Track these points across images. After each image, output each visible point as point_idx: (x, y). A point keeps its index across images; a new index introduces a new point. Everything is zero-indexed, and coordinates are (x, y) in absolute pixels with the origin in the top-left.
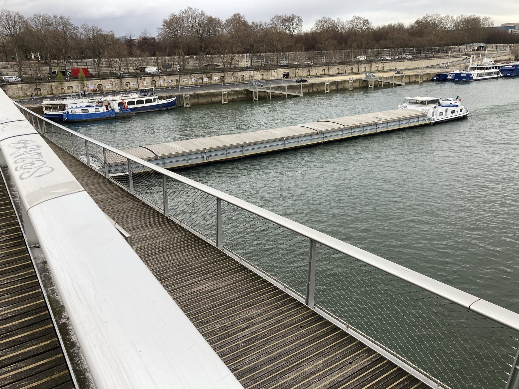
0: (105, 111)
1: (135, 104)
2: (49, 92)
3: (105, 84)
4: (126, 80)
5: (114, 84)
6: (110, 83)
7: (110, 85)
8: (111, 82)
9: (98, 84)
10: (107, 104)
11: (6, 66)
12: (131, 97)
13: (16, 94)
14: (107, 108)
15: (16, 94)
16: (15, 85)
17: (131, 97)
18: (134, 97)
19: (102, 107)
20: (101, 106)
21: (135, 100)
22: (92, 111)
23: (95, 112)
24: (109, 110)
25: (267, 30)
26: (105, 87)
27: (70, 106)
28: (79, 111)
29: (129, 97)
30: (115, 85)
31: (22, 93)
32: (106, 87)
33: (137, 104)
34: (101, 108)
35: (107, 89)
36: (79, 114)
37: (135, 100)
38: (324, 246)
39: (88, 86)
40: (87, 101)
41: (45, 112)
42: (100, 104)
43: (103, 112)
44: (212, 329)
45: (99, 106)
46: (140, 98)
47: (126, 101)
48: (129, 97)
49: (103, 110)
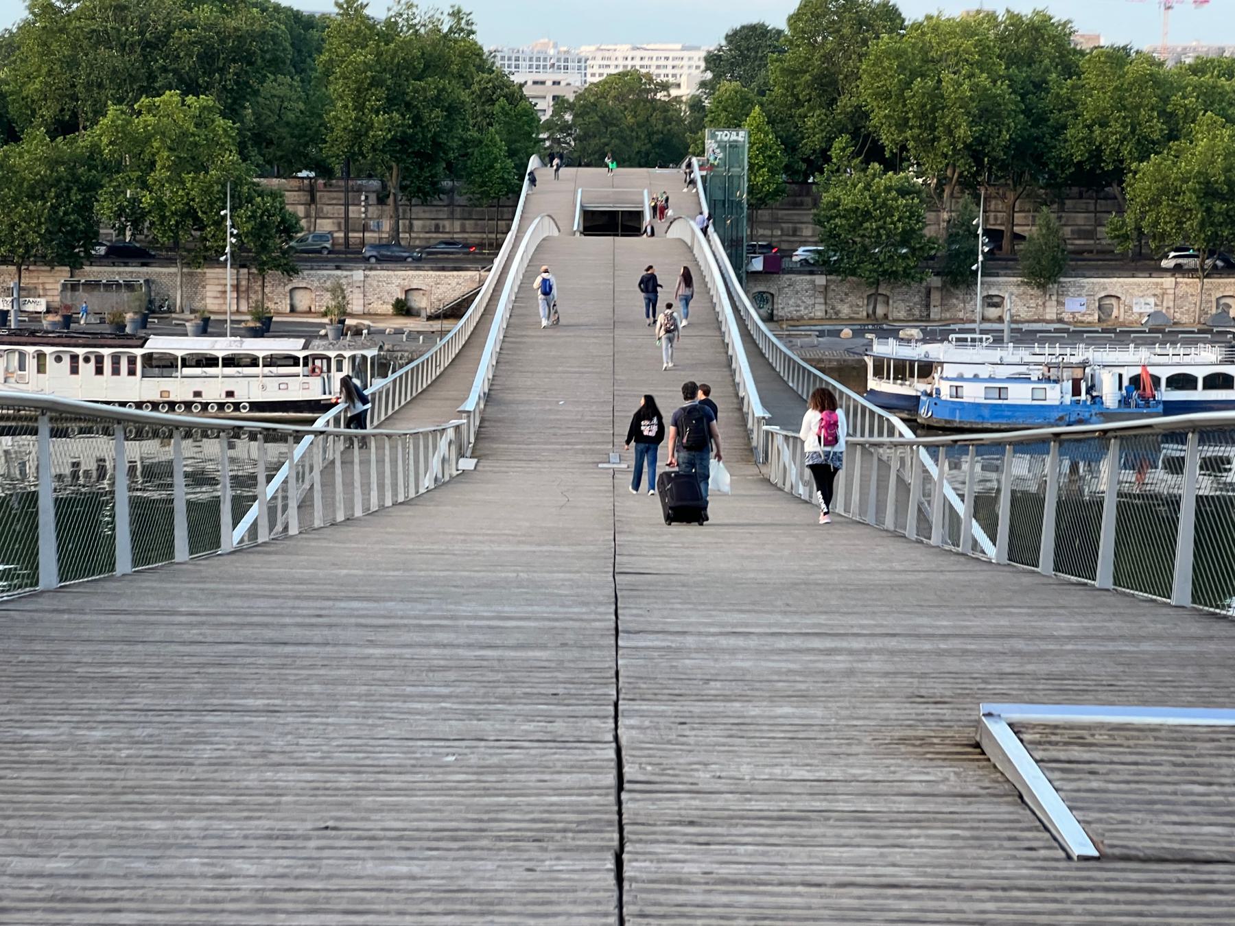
0: (1068, 399)
1: (1195, 388)
2: (917, 312)
3: (1131, 294)
4: (1226, 285)
5: (1172, 297)
6: (1155, 295)
7: (1152, 300)
8: (1159, 291)
9: (1103, 294)
10: (1078, 373)
11: (798, 199)
12: (1187, 359)
13: (806, 308)
14: (1076, 391)
15: (806, 308)
16: (808, 277)
17: (1187, 359)
18: (1198, 360)
19: (1058, 386)
20: (1056, 381)
21: (1200, 373)
22: (1019, 394)
23: (1029, 402)
24: (1083, 396)
25: (477, 52)
26: (1131, 308)
27: (949, 371)
28: (973, 393)
29: (1176, 359)
30: (1171, 304)
31: (823, 307)
32: (1136, 309)
33: (1205, 387)
34: (1053, 389)
35: (1135, 317)
36: (972, 400)
37: (1200, 373)
38: (1095, 838)
39: (1061, 299)
40: (1017, 360)
41: (873, 383)
42: (1054, 373)
43: (1057, 403)
44: (14, 418)
45: (1048, 380)
46: (1222, 363)
47: (1164, 373)
48: (1176, 359)
49: (1055, 395)
